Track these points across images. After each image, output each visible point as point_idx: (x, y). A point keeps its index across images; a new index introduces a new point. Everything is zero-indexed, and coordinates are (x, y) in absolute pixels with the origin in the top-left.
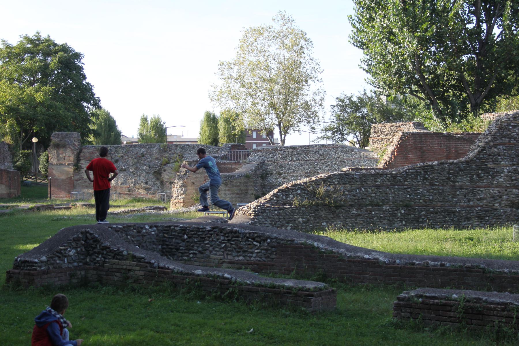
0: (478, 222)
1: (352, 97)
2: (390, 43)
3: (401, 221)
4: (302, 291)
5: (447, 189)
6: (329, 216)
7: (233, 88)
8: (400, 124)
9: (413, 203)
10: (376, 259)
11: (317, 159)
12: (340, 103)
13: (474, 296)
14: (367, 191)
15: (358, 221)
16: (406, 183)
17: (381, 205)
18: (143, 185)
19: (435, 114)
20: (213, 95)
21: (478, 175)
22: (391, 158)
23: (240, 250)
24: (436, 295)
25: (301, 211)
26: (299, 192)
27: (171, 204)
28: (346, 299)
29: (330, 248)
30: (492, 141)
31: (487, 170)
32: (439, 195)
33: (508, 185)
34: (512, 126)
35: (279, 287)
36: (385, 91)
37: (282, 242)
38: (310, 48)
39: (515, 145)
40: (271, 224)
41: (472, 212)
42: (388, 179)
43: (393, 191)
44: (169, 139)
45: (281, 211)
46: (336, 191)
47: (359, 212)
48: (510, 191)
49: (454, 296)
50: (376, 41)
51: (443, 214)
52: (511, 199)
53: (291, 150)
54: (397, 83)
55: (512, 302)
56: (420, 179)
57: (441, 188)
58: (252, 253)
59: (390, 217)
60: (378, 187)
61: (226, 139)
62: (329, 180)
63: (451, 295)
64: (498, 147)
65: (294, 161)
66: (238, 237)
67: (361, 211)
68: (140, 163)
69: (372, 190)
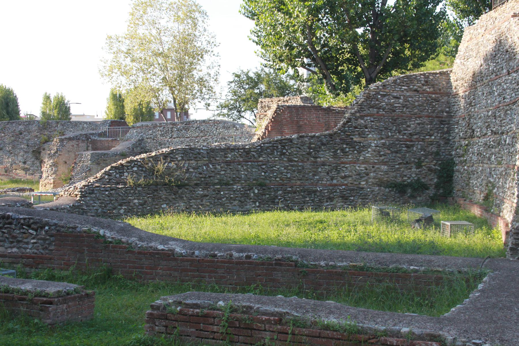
0: (343, 202)
1: (248, 72)
2: (280, 13)
3: (254, 202)
4: (40, 296)
5: (308, 165)
6: (170, 197)
7: (123, 63)
8: (288, 99)
9: (268, 182)
10: (171, 250)
11: (198, 136)
12: (236, 78)
13: (244, 304)
14: (216, 168)
15: (204, 202)
16: (261, 159)
17: (232, 184)
18: (21, 165)
19: (328, 89)
20: (104, 70)
21: (343, 150)
22: (265, 133)
23: (15, 240)
24: (199, 302)
25: (137, 192)
26: (135, 169)
27: (40, 185)
28: (109, 303)
29: (118, 237)
30: (359, 112)
31: (352, 144)
32: (298, 173)
33: (376, 161)
34: (381, 95)
35: (13, 290)
36: (275, 64)
37: (62, 229)
38: (205, 20)
39: (384, 116)
40: (100, 207)
41: (335, 192)
42: (240, 155)
43: (245, 168)
44: (73, 119)
45: (113, 192)
46: (178, 167)
47: (206, 192)
48: (378, 168)
49: (221, 303)
50: (265, 11)
51: (302, 194)
52: (379, 176)
53: (171, 126)
54: (288, 56)
55: (289, 311)
56: (277, 155)
57: (300, 164)
58: (27, 243)
59: (241, 197)
60: (228, 163)
61: (132, 118)
62: (172, 156)
63: (217, 302)
64: (366, 118)
65: (174, 138)
66: (10, 223)
67: (208, 191)
68: (18, 141)
69: (221, 167)
